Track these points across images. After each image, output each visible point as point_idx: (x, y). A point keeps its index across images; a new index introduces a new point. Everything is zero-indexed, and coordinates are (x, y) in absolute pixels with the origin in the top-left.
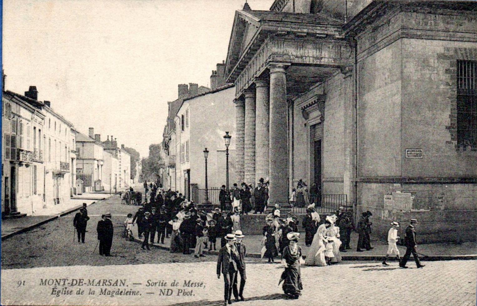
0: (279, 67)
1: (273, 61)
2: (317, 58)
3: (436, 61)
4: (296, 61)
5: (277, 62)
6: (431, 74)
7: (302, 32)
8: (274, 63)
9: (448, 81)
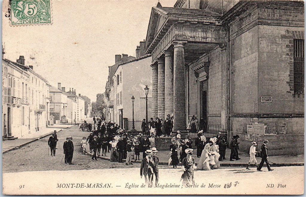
0: (180, 44)
1: (176, 40)
2: (204, 38)
3: (280, 39)
4: (191, 40)
5: (179, 40)
6: (277, 48)
7: (194, 21)
8: (177, 41)
9: (288, 52)
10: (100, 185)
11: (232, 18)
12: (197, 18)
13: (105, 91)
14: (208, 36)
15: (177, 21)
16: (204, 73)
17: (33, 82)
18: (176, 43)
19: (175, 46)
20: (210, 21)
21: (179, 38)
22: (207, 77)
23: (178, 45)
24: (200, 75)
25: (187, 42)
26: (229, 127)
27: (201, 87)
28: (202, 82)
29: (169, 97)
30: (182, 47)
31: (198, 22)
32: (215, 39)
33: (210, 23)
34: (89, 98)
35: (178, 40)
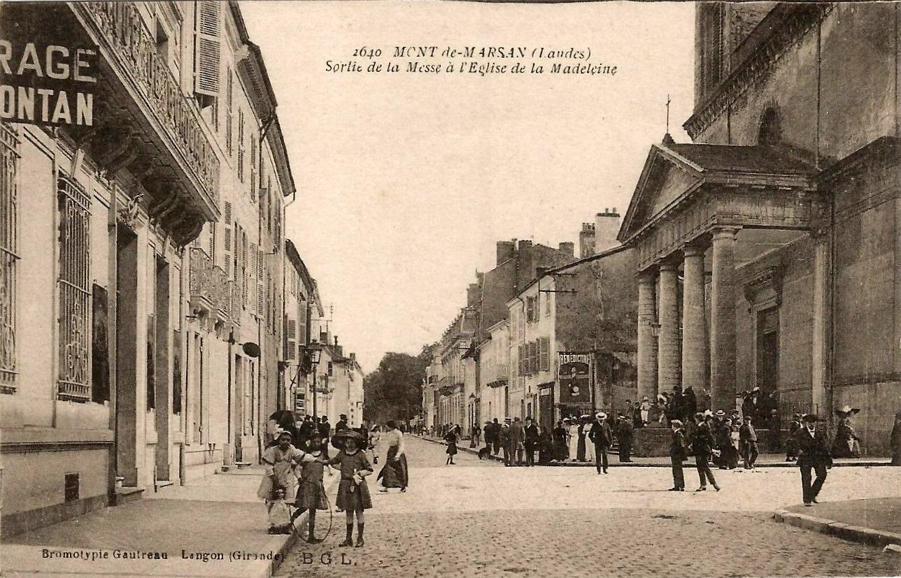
0: (727, 231)
1: (718, 224)
10: (497, 51)
11: (841, 180)
12: (764, 178)
13: (622, 203)
14: (786, 214)
15: (720, 185)
16: (772, 292)
17: (219, 130)
18: (719, 230)
19: (714, 237)
20: (792, 184)
21: (725, 219)
22: (779, 303)
23: (723, 235)
24: (760, 297)
25: (741, 227)
26: (833, 409)
27: (762, 323)
28: (763, 314)
29: (368, 455)
30: (731, 238)
31: (767, 186)
32: (803, 221)
33: (792, 187)
34: (530, 467)
35: (723, 224)
